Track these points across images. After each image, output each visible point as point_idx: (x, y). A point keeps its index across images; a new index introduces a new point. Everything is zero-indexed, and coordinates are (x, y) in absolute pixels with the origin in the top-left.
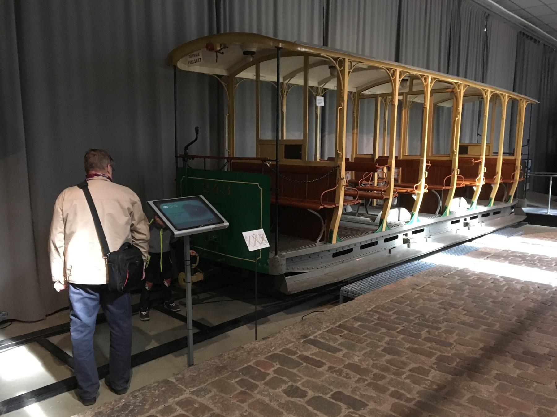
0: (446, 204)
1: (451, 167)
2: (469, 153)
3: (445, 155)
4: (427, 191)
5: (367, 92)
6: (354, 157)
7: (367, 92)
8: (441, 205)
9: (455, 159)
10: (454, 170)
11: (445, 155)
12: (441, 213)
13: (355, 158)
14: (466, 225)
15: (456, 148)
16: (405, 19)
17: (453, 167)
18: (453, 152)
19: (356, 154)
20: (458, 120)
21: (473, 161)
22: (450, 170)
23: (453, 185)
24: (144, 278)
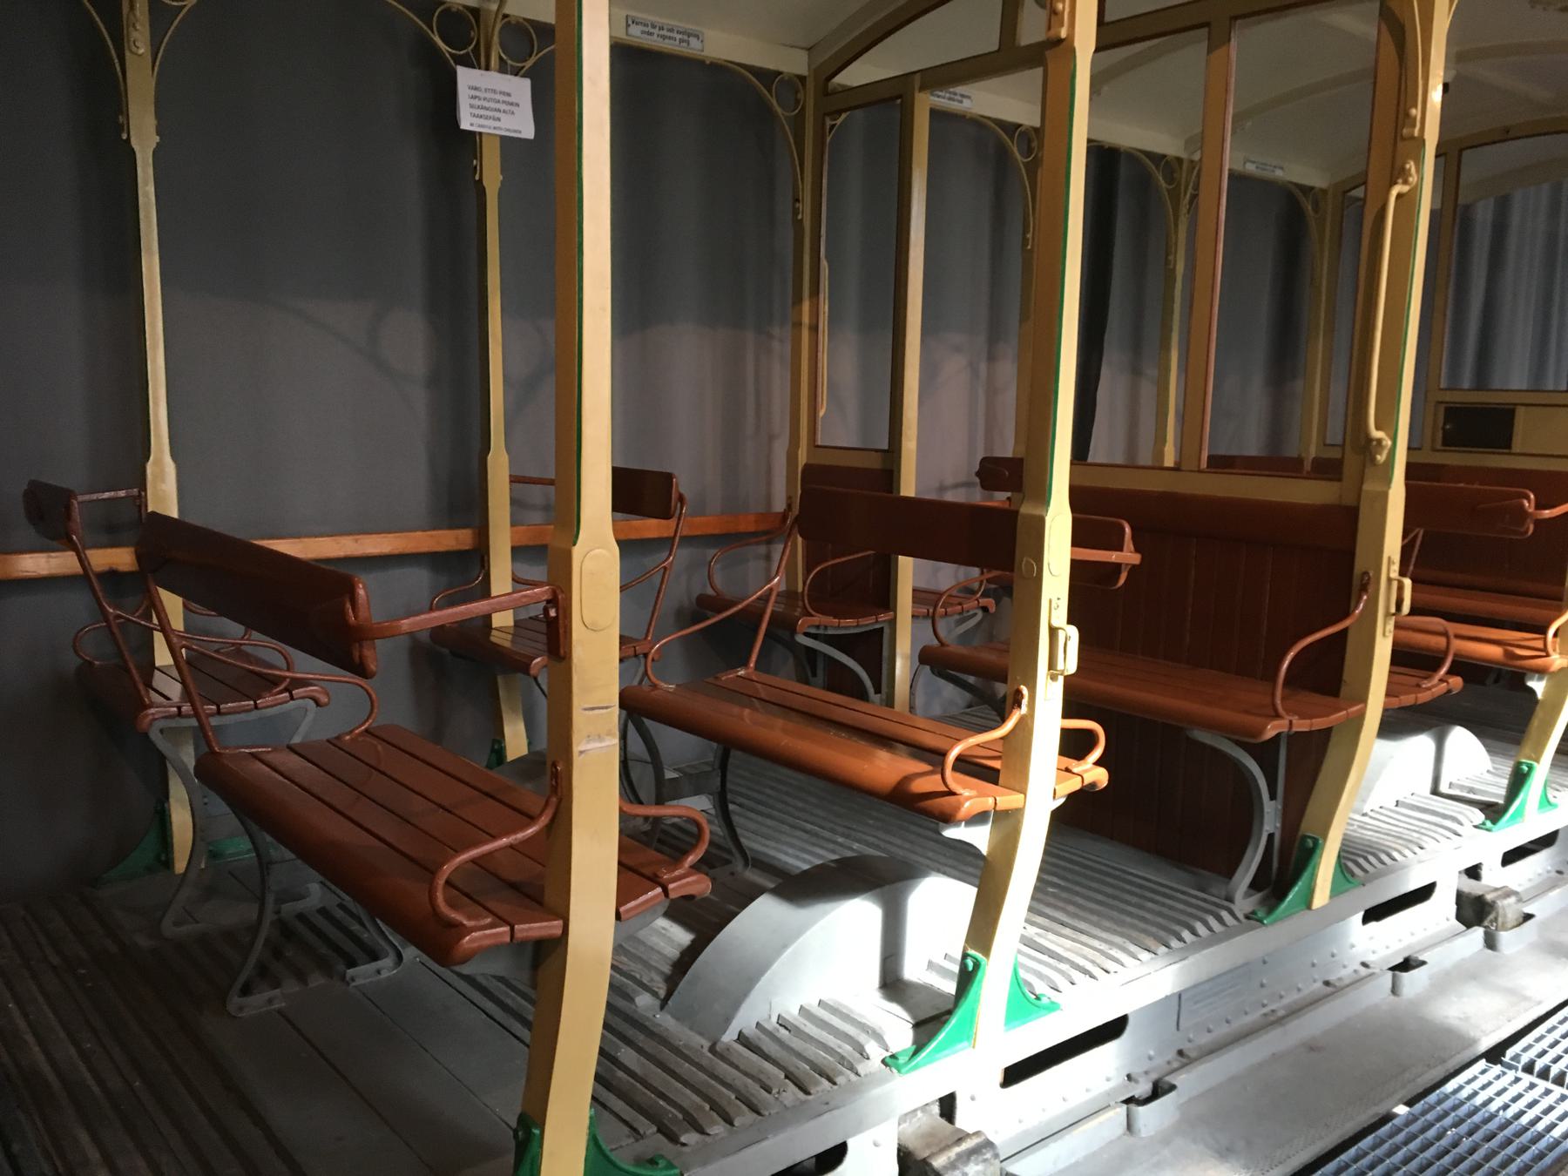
0: (1306, 827)
1: (1350, 554)
2: (1516, 448)
3: (1327, 469)
4: (1101, 776)
5: (857, 75)
6: (802, 459)
7: (857, 75)
8: (1271, 820)
9: (1383, 498)
10: (1367, 584)
11: (1327, 469)
12: (1282, 876)
13: (807, 467)
14: (1473, 910)
15: (1387, 419)
16: (1454, 257)
17: (1360, 565)
18: (1367, 447)
19: (814, 446)
20: (1408, 203)
21: (1528, 505)
22: (1336, 576)
23: (1363, 698)
24: (1122, 581)
